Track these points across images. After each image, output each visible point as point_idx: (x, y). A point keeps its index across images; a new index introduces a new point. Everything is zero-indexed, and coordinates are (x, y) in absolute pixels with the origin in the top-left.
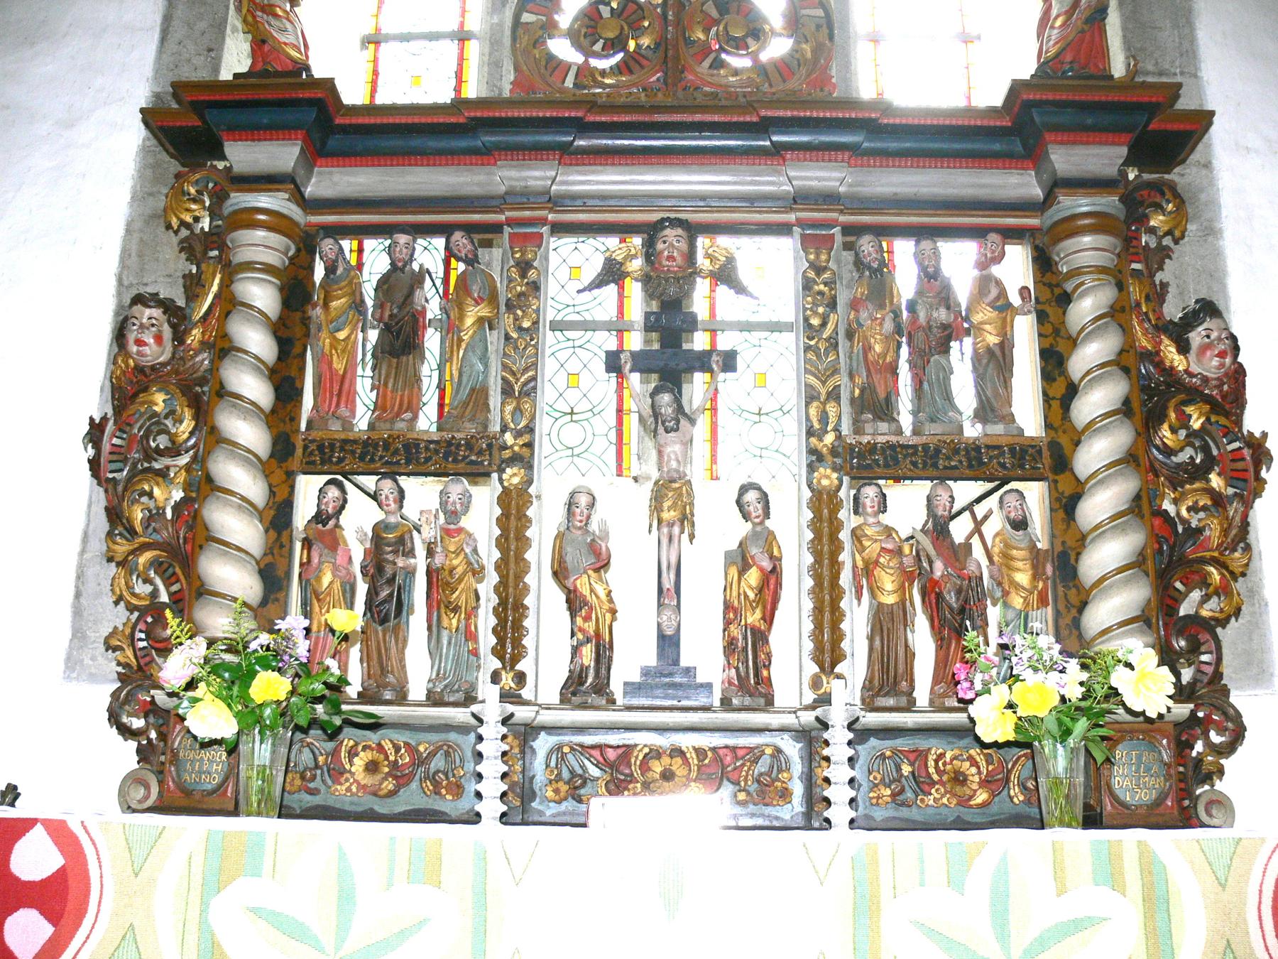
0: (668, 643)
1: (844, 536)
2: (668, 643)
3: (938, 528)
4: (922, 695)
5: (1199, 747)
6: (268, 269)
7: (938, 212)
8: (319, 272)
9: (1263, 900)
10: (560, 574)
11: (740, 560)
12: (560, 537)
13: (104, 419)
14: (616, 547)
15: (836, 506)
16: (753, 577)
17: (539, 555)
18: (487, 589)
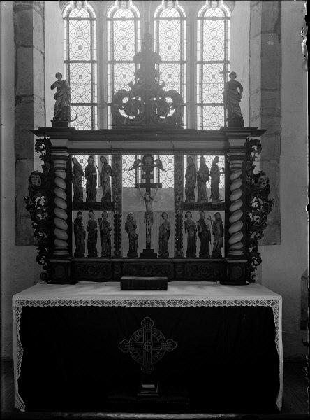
0: (148, 245)
1: (183, 223)
2: (148, 245)
3: (202, 221)
4: (198, 255)
5: (252, 264)
6: (63, 169)
7: (139, 43)
8: (73, 165)
9: (167, 147)
10: (127, 229)
11: (162, 228)
12: (126, 224)
13: (28, 198)
14: (138, 224)
15: (181, 216)
16: (165, 232)
17: (123, 227)
18: (112, 233)
